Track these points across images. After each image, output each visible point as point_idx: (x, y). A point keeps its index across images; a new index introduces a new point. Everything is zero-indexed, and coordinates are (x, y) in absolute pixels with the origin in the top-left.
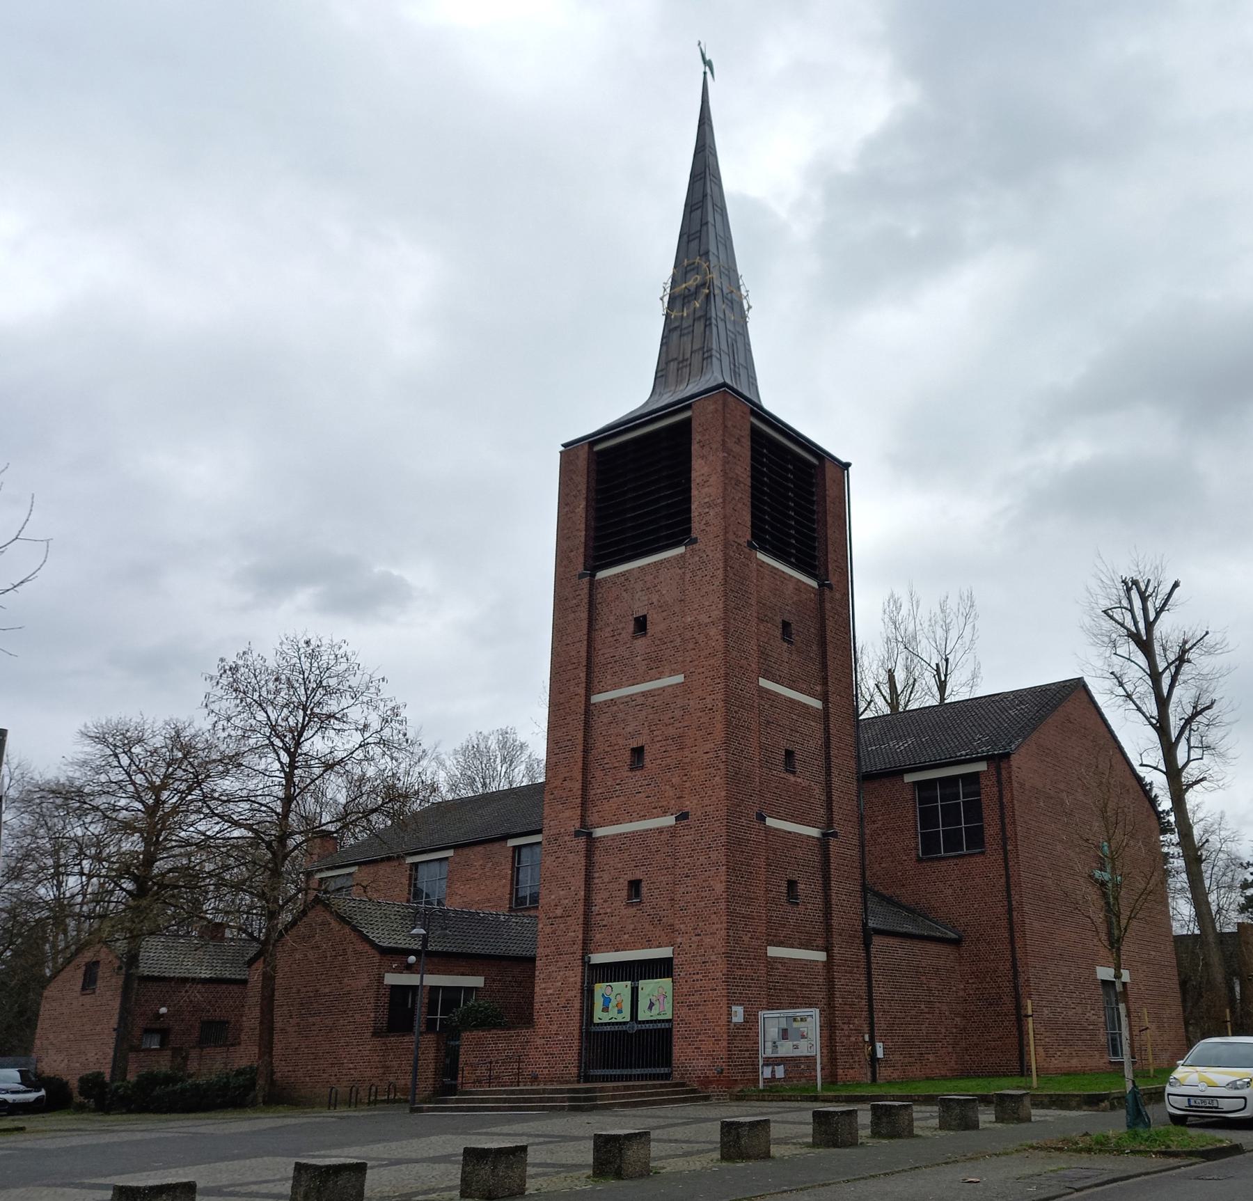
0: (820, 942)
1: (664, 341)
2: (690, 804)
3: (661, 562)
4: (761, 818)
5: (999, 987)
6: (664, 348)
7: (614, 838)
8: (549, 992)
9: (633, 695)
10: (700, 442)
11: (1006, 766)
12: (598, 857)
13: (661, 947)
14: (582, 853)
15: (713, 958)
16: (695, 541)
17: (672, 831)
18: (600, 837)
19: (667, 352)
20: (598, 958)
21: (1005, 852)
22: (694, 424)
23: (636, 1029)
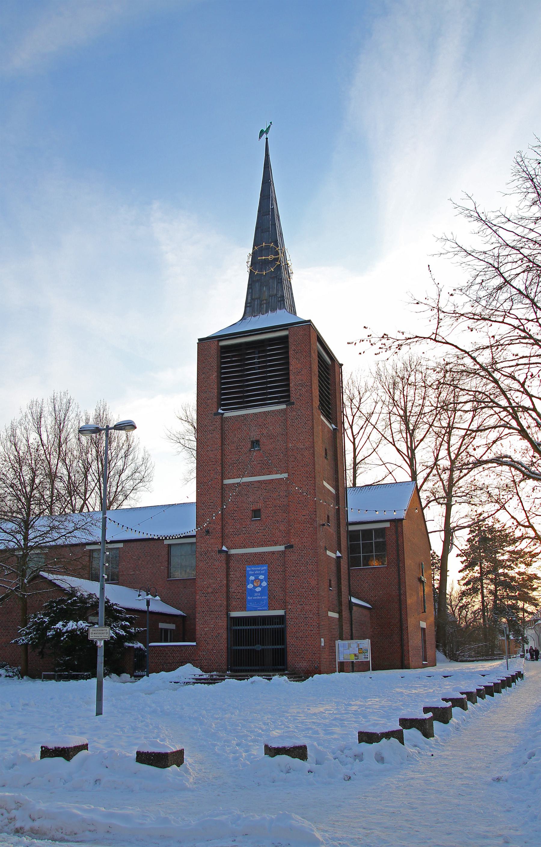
0: (337, 609)
1: (250, 286)
2: (293, 541)
3: (269, 412)
4: (326, 549)
5: (391, 630)
6: (250, 291)
7: (237, 555)
8: (206, 629)
9: (252, 482)
10: (294, 350)
11: (400, 525)
12: (231, 564)
13: (276, 610)
14: (224, 562)
15: (311, 616)
16: (293, 403)
17: (283, 552)
18: (234, 554)
19: (252, 293)
20: (234, 614)
21: (399, 567)
22: (291, 340)
23: (256, 647)
